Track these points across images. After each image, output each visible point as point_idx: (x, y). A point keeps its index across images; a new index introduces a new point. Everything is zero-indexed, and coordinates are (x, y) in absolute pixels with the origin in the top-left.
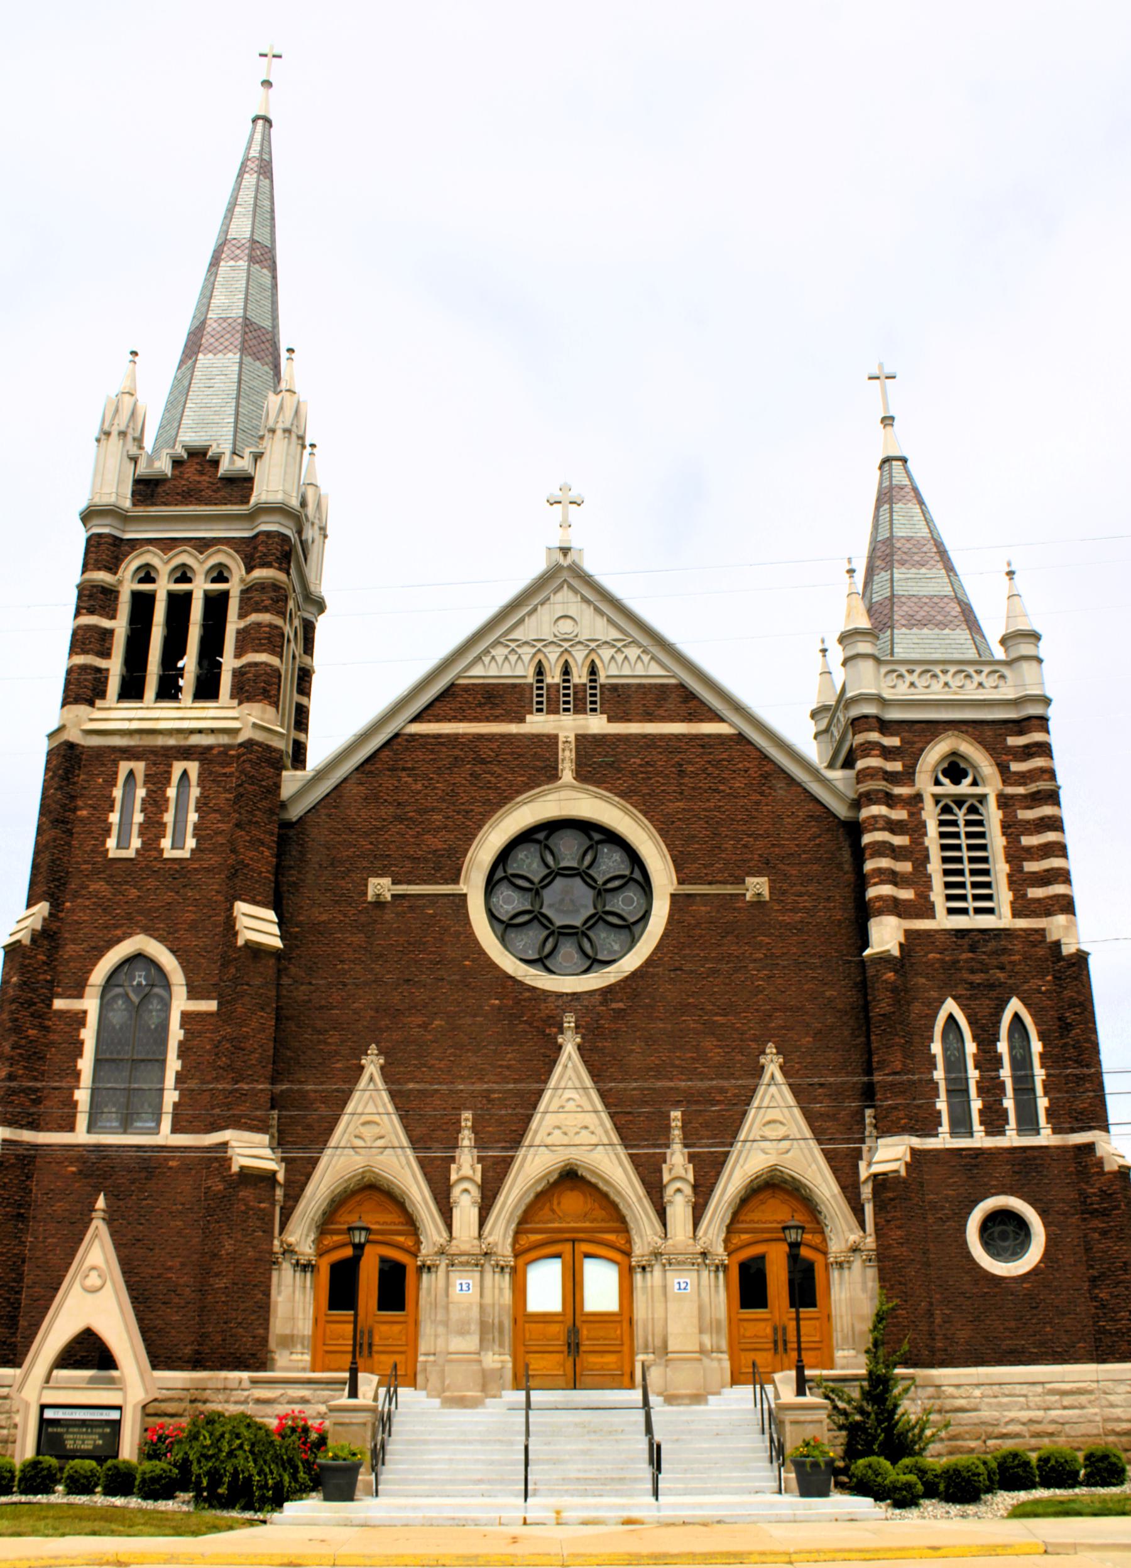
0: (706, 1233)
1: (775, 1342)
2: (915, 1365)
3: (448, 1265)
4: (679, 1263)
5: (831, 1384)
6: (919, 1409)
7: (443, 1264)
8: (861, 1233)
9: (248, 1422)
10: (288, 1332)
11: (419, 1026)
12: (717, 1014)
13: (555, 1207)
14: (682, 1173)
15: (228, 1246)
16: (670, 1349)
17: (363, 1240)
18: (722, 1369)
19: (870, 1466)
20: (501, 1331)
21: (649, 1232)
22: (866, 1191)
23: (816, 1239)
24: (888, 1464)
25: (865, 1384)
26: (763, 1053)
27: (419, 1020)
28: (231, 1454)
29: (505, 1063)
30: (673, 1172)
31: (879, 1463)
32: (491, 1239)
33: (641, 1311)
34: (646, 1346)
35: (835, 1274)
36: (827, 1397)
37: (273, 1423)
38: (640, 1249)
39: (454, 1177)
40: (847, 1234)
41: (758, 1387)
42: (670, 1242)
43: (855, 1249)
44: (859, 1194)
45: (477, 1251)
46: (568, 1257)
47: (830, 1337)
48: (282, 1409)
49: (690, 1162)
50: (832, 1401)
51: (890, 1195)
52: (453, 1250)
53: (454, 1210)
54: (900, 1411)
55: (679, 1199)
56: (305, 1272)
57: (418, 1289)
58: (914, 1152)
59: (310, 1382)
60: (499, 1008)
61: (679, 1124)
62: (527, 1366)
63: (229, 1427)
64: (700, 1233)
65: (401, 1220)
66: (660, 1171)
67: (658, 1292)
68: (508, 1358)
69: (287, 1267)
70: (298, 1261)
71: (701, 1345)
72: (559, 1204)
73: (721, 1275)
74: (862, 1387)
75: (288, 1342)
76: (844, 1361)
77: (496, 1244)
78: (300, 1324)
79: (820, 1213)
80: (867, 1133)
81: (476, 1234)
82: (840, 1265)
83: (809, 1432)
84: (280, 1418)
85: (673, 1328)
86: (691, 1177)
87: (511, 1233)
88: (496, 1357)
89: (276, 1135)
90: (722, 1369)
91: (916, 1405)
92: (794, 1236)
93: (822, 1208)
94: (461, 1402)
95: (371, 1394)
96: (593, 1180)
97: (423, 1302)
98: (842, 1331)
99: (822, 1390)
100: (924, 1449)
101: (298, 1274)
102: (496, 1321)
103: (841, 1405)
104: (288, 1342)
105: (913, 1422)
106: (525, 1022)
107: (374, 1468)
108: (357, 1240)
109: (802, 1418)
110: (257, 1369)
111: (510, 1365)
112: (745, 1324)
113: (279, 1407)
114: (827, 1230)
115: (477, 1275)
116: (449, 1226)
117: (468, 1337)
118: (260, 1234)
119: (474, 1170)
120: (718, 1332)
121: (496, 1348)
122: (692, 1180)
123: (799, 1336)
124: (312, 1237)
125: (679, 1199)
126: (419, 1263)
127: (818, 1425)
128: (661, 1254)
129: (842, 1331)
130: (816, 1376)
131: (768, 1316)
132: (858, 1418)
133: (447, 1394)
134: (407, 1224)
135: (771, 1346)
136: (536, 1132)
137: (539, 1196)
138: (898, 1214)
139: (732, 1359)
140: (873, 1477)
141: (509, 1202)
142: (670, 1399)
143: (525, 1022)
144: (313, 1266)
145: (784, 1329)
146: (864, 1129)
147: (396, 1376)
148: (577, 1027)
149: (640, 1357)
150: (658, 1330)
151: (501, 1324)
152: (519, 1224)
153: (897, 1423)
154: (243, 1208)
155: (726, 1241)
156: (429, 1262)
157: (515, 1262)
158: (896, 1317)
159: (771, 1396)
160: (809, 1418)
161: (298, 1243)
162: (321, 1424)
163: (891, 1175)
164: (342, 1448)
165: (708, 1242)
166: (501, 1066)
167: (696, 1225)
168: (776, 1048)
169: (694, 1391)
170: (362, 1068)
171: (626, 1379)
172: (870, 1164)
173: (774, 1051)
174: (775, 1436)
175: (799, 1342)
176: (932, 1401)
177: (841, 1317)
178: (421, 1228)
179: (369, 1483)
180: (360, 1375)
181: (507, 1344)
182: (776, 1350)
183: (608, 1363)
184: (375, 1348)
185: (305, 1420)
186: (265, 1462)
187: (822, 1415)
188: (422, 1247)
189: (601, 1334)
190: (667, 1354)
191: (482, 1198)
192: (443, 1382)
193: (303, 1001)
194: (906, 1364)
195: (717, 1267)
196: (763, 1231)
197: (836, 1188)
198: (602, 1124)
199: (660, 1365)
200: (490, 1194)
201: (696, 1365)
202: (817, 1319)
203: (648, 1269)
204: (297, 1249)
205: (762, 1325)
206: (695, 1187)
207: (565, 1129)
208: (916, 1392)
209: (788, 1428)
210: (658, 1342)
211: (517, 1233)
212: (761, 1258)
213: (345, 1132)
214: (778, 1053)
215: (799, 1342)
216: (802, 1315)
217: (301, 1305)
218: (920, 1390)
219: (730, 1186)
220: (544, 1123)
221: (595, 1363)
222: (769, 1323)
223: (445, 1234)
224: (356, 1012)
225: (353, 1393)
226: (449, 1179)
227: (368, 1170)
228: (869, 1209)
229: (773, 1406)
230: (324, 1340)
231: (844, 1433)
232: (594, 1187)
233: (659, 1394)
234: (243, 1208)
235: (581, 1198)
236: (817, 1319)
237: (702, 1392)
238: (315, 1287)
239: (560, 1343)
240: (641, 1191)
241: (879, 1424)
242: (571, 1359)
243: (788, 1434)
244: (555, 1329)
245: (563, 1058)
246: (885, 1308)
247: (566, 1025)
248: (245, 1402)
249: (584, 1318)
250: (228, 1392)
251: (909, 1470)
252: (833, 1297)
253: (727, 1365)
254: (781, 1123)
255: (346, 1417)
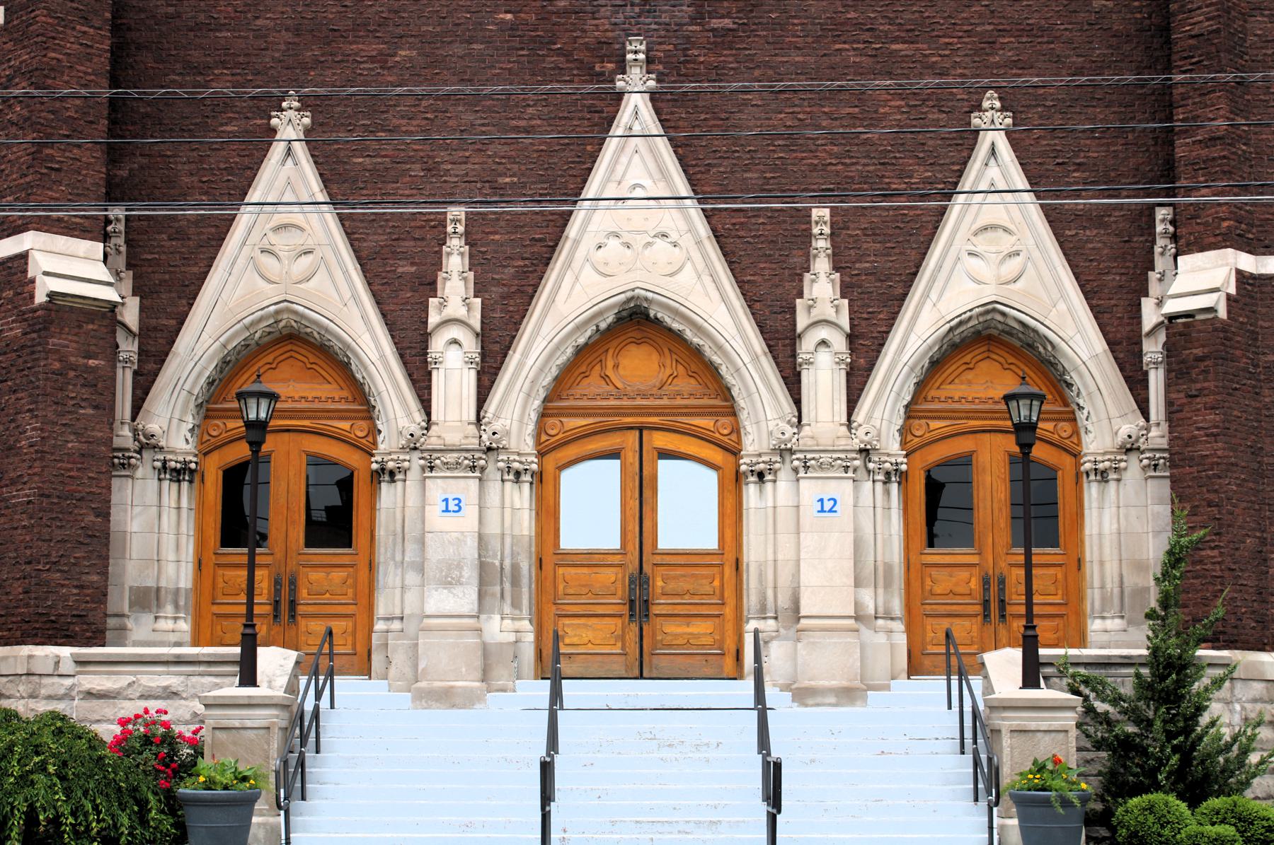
0: (869, 417)
1: (986, 604)
2: (1231, 644)
3: (423, 469)
4: (821, 467)
5: (1082, 671)
6: (1237, 719)
7: (416, 462)
8: (1142, 422)
9: (59, 725)
10: (151, 583)
11: (372, 59)
12: (896, 40)
13: (609, 372)
14: (830, 314)
15: (32, 432)
16: (803, 613)
17: (263, 415)
18: (892, 646)
19: (1151, 808)
20: (515, 582)
21: (400, 413)
22: (1153, 349)
23: (1065, 428)
24: (1183, 806)
25: (1145, 671)
26: (978, 107)
27: (374, 48)
28: (25, 780)
29: (522, 123)
30: (814, 312)
31: (1166, 804)
32: (497, 426)
33: (755, 550)
34: (763, 608)
35: (1092, 491)
36: (1076, 692)
37: (108, 731)
38: (754, 443)
39: (433, 319)
40: (1116, 422)
41: (955, 679)
42: (806, 431)
43: (1129, 449)
44: (1140, 354)
45: (473, 443)
46: (633, 458)
47: (1081, 598)
48: (129, 708)
49: (843, 296)
50: (1086, 698)
51: (1198, 352)
52: (433, 441)
53: (434, 373)
54: (1205, 719)
55: (824, 360)
56: (179, 481)
57: (373, 509)
58: (1242, 277)
59: (179, 661)
60: (513, 27)
61: (827, 230)
62: (557, 638)
63: (21, 735)
64: (860, 416)
65: (345, 394)
66: (793, 310)
67: (785, 517)
68: (526, 625)
69: (145, 470)
70: (165, 462)
71: (857, 605)
72: (616, 366)
73: (894, 487)
74: (1138, 676)
75: (148, 599)
76: (1105, 637)
77: (508, 433)
78: (170, 569)
79: (1070, 385)
80: (1157, 250)
81: (473, 418)
82: (1103, 475)
83: (1045, 748)
84: (123, 722)
85: (808, 577)
86: (845, 322)
87: (534, 416)
88: (507, 622)
89: (123, 249)
90: (892, 646)
91: (1232, 711)
92: (1024, 412)
93: (1075, 378)
94: (446, 698)
95: (283, 681)
96: (676, 326)
97: (381, 533)
98: (1102, 587)
99: (1065, 681)
100: (1247, 784)
101: (166, 484)
102: (507, 563)
103: (1101, 707)
104: (148, 599)
105: (1227, 737)
106: (560, 52)
107: (281, 806)
108: (252, 416)
109: (1033, 725)
110: (88, 643)
111: (530, 638)
112: (934, 572)
113: (127, 704)
114: (1081, 416)
115: (474, 484)
116: (426, 404)
117: (458, 590)
118: (90, 411)
119: (470, 309)
120: (888, 585)
121: (507, 609)
122: (847, 328)
123: (1029, 593)
124: (190, 421)
125: (824, 360)
126: (375, 466)
127: (1061, 735)
128: (791, 452)
129: (1102, 587)
130: (1058, 656)
131: (975, 559)
132: (1131, 729)
133: (423, 684)
134: (362, 405)
135: (978, 609)
136: (577, 242)
137: (581, 352)
138: (1211, 385)
139: (909, 631)
140: (1156, 828)
141: (530, 362)
142: (803, 695)
143: (560, 52)
144: (192, 472)
145: (1002, 581)
146: (1154, 242)
147: (331, 655)
148: (649, 61)
149: (751, 626)
150: (784, 580)
151: (515, 568)
152: (546, 400)
153: (1200, 738)
154: (57, 365)
155: (904, 431)
156: (391, 465)
157: (540, 464)
158: (1201, 562)
159: (978, 693)
160: (1044, 725)
161: (166, 433)
162: (195, 732)
163: (1199, 317)
164: (223, 769)
165: (874, 432)
166: (517, 129)
167: (852, 402)
168: (1000, 99)
169: (845, 683)
170: (274, 131)
171: (729, 661)
172: (1160, 303)
173: (998, 104)
174: (983, 757)
175: (1029, 604)
176: (1259, 706)
177: (1102, 563)
178: (379, 407)
179: (274, 830)
180: (261, 651)
181: (525, 602)
182: (986, 617)
183: (697, 636)
184: (301, 609)
185: (166, 725)
186: (86, 793)
187: (1069, 720)
188: (380, 438)
189: (683, 585)
190: (799, 619)
191: (483, 355)
192: (416, 666)
193: (168, 16)
194: (1216, 642)
195: (888, 474)
196: (970, 414)
197: (1099, 344)
198: (692, 230)
199: (786, 639)
200: (496, 347)
201: (850, 639)
202: (1060, 565)
203: (768, 477)
204: (162, 443)
205: (963, 574)
206: (851, 338)
207: (626, 237)
208: (1232, 689)
209: (1006, 741)
210: (784, 601)
211: (544, 414)
212: (965, 461)
213: (244, 243)
214: (1003, 109)
215: (1029, 604)
216: (1035, 560)
217: (172, 537)
218: (1239, 685)
219: (913, 337)
220: (591, 228)
221: (676, 636)
222: (976, 571)
223: (419, 417)
224: (260, 34)
225: (249, 678)
226: (426, 323)
227: (284, 308)
228: (1156, 381)
229: (981, 707)
230: (214, 598)
231: (1104, 754)
232: (677, 337)
233: (786, 688)
234: (57, 365)
235: (655, 356)
236: (1060, 565)
237: (857, 683)
238: (200, 508)
239: (617, 602)
240: (758, 344)
241: (1169, 739)
242: (634, 628)
243: (1006, 751)
244: (609, 575)
245: (624, 118)
246: (1184, 541)
247: (630, 57)
248: (67, 696)
249: (658, 559)
250: (36, 679)
251: (1218, 817)
252: (1087, 531)
253: (901, 640)
254: (1006, 230)
255: (234, 717)
